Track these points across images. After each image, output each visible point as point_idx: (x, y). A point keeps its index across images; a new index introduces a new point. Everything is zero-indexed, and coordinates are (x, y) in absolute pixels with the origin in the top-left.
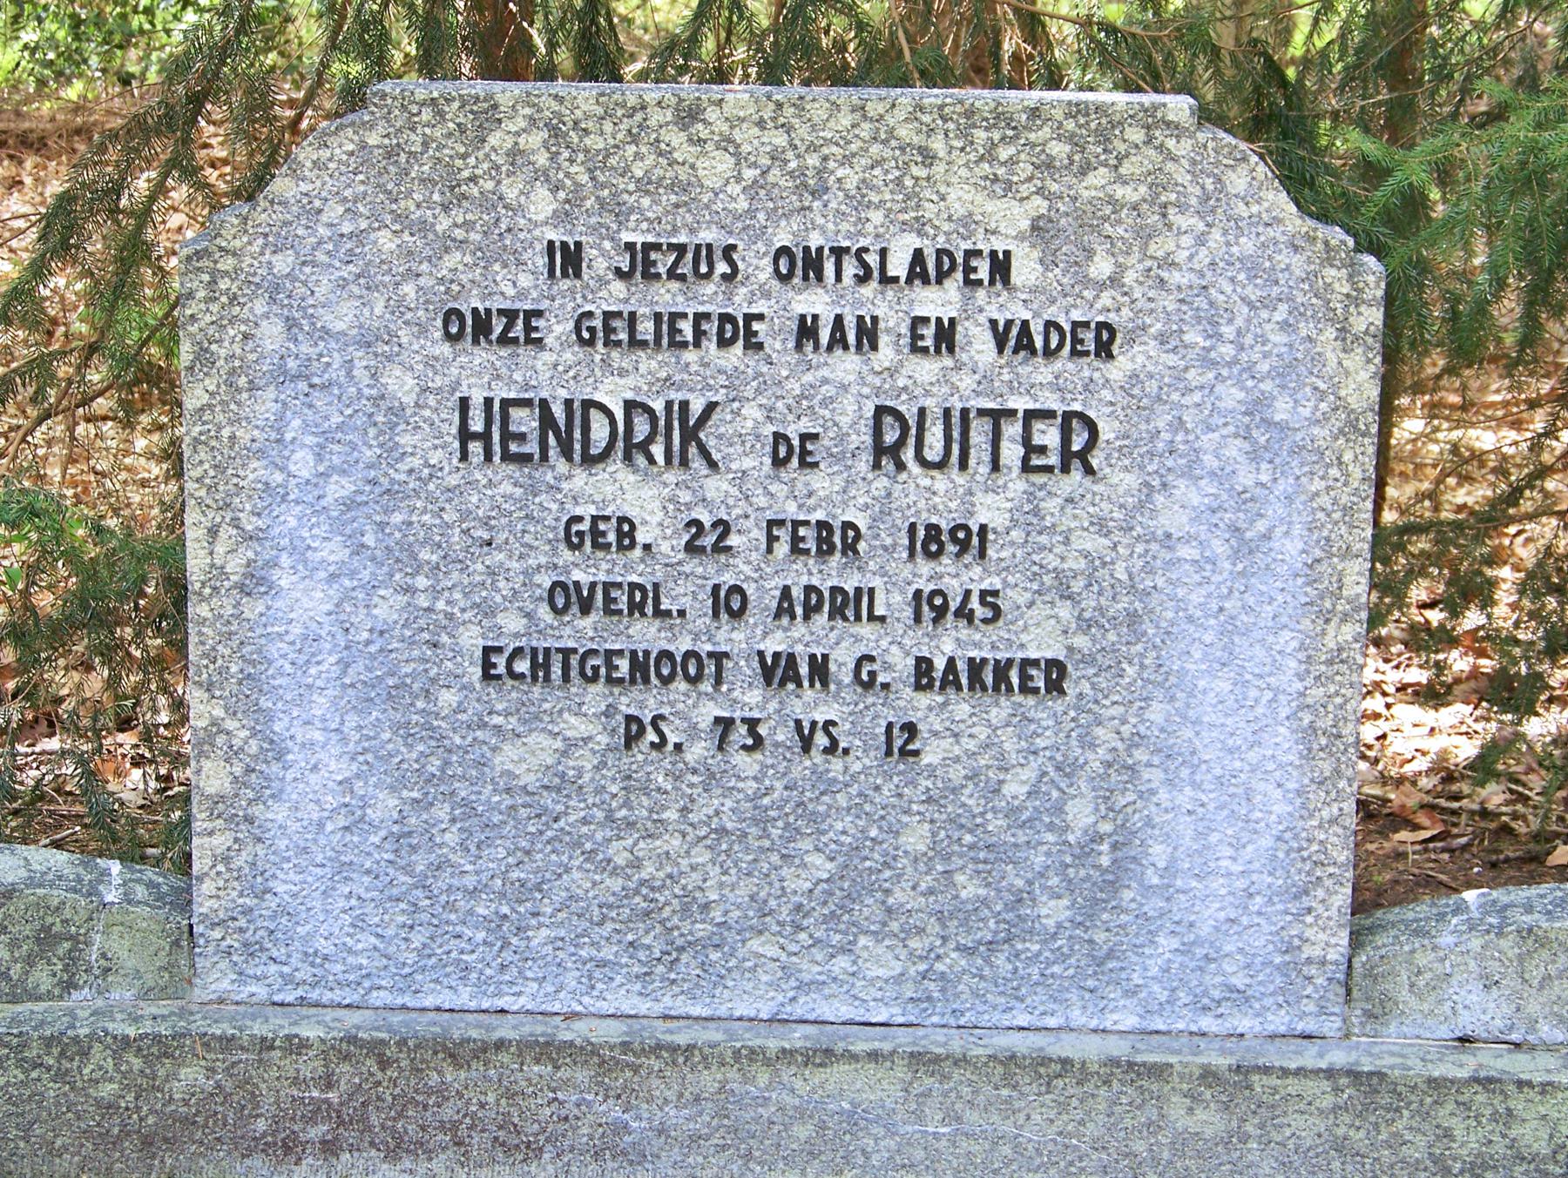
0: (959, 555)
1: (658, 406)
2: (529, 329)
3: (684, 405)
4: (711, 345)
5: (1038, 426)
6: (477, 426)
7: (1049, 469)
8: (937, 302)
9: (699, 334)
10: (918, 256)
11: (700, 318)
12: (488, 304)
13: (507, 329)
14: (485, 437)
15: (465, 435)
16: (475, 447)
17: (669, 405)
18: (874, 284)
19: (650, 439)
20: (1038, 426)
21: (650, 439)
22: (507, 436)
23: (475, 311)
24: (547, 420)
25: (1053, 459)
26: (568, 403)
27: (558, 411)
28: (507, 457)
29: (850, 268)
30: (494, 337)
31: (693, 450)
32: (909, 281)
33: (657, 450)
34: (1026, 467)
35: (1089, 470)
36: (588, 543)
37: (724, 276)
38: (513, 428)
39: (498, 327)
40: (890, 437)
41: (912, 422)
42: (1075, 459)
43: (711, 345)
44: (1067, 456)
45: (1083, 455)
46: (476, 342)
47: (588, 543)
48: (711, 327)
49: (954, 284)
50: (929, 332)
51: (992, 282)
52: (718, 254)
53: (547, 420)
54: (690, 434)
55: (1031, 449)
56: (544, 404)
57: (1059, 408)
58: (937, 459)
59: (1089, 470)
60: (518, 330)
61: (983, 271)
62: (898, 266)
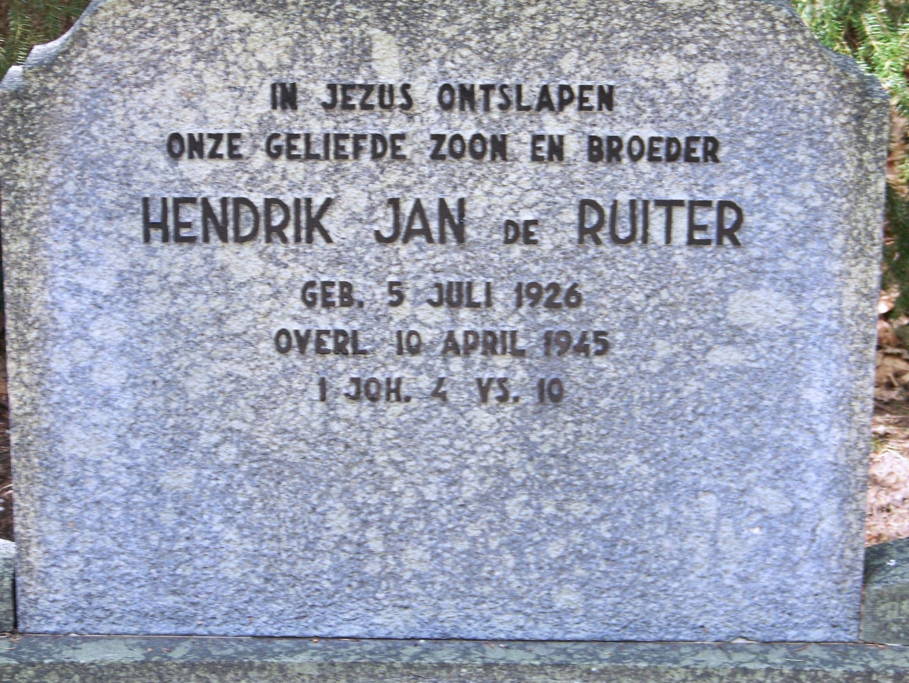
0: (532, 305)
1: (289, 201)
2: (232, 148)
3: (309, 201)
4: (366, 158)
5: (698, 211)
6: (155, 218)
7: (707, 242)
8: (551, 125)
9: (358, 150)
10: (545, 90)
11: (358, 138)
12: (201, 131)
13: (215, 147)
14: (162, 225)
15: (148, 225)
16: (156, 233)
17: (297, 201)
18: (513, 110)
19: (284, 224)
20: (698, 211)
21: (284, 224)
22: (179, 225)
23: (191, 136)
24: (208, 211)
25: (712, 234)
26: (224, 201)
27: (217, 209)
28: (179, 239)
29: (496, 99)
30: (207, 151)
31: (316, 234)
32: (539, 108)
33: (289, 232)
34: (691, 241)
35: (736, 243)
36: (319, 302)
37: (402, 106)
38: (697, 223)
39: (209, 144)
40: (277, 220)
41: (607, 212)
42: (729, 234)
43: (366, 158)
44: (722, 232)
45: (730, 234)
46: (191, 157)
47: (319, 302)
48: (367, 144)
49: (571, 110)
50: (544, 145)
51: (600, 109)
52: (397, 93)
53: (208, 211)
54: (314, 223)
55: (693, 227)
56: (205, 201)
57: (685, 197)
58: (628, 234)
59: (736, 243)
60: (223, 149)
61: (593, 99)
62: (530, 96)
